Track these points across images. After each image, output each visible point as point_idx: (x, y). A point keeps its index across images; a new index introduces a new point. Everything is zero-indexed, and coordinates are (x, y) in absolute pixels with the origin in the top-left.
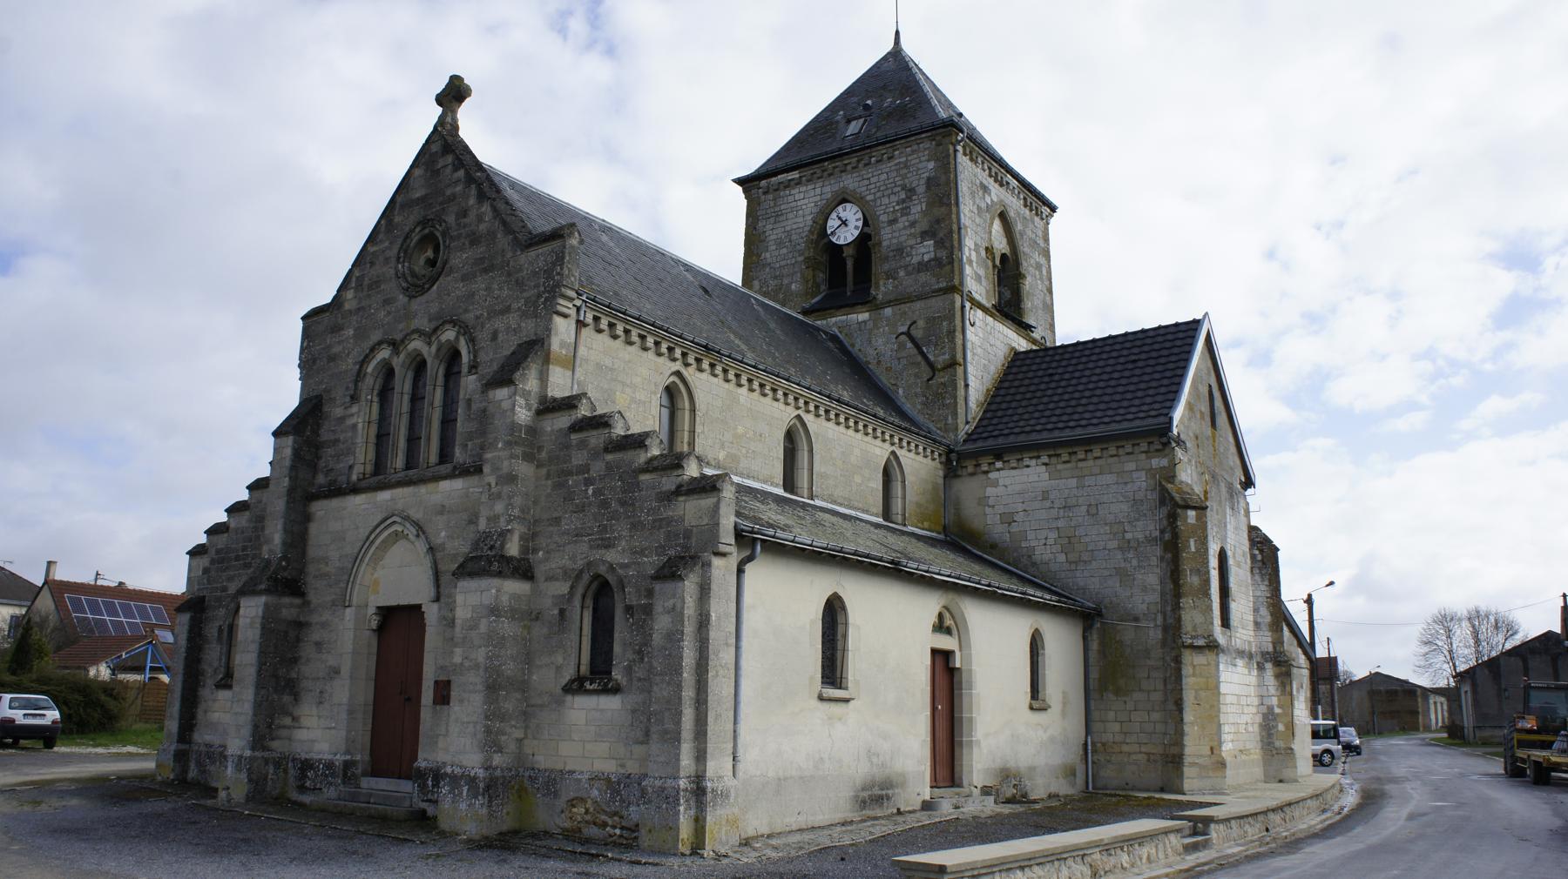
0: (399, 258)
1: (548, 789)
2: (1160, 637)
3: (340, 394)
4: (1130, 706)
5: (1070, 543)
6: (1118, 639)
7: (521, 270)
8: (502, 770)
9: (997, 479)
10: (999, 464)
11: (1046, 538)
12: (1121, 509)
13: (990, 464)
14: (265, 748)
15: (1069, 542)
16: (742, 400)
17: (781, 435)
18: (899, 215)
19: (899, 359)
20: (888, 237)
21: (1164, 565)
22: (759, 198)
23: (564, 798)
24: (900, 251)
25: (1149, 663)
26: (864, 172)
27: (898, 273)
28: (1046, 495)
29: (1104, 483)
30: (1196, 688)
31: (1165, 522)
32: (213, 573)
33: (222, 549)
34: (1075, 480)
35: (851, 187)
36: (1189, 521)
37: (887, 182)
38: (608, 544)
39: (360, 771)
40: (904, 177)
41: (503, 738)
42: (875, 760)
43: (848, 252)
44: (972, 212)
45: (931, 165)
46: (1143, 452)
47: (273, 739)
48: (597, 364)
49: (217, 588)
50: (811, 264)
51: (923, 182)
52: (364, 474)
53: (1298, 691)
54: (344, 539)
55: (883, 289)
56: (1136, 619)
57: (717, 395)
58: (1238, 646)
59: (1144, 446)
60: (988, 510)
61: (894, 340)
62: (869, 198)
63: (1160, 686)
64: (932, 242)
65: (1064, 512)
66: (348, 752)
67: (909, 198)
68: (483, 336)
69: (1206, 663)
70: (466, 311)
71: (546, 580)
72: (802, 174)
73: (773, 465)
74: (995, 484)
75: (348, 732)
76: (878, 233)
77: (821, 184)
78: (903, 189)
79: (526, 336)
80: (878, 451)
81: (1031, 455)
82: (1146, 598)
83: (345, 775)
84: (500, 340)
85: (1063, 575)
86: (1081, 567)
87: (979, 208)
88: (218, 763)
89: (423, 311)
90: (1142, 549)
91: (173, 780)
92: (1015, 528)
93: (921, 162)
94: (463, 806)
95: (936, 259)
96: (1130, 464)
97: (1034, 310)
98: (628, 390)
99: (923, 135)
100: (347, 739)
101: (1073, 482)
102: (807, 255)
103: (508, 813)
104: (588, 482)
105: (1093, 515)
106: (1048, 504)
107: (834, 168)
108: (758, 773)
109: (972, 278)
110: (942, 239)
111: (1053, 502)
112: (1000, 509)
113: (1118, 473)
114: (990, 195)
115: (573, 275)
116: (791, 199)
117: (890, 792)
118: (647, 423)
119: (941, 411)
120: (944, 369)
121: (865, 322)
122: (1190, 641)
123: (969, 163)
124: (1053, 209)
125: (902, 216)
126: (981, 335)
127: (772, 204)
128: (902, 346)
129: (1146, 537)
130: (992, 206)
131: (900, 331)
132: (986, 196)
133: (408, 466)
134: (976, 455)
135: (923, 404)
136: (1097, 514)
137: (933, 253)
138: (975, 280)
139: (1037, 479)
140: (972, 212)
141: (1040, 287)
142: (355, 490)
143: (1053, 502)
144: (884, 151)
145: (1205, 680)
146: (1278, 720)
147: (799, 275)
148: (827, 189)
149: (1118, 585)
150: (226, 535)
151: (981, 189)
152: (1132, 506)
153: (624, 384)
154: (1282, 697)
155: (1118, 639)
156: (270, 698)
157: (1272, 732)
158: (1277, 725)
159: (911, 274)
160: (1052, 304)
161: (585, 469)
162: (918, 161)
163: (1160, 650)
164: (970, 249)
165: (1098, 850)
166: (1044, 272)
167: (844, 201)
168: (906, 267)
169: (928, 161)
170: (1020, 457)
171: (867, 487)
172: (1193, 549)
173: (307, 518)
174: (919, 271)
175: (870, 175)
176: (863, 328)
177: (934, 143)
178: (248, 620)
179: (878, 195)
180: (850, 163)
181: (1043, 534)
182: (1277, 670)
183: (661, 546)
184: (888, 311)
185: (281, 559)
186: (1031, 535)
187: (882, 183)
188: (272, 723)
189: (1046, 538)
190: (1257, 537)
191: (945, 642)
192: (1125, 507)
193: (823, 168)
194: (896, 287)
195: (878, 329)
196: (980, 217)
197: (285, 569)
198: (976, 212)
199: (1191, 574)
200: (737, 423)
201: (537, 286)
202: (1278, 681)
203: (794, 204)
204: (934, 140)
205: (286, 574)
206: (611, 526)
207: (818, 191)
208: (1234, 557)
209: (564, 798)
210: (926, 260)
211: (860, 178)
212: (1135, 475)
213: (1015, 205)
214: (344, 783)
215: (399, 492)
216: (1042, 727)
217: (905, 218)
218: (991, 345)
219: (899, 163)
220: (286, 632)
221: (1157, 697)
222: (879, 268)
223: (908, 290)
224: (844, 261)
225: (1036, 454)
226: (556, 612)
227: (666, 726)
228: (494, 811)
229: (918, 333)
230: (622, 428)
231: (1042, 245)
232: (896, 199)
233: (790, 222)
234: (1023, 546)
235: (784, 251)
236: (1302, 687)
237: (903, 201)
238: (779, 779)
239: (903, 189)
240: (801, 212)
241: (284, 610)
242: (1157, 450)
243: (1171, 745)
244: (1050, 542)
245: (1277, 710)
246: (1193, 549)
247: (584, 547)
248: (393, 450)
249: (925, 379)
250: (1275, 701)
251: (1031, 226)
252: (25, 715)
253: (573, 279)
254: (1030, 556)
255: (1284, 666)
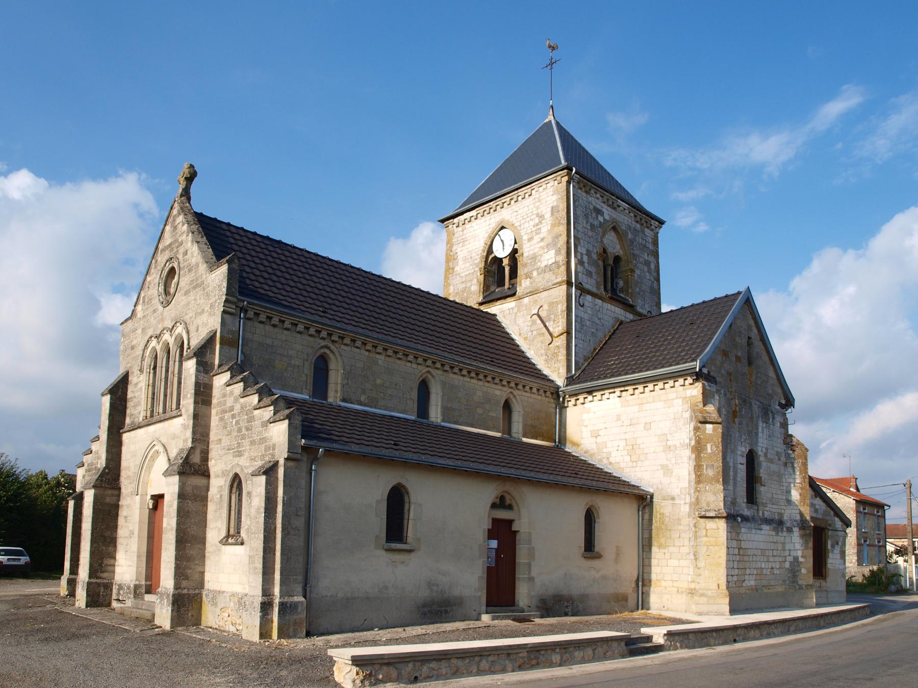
1: (213, 602)
2: (688, 510)
4: (668, 556)
6: (661, 511)
7: (208, 286)
14: (98, 578)
15: (633, 448)
16: (380, 362)
18: (534, 234)
19: (532, 331)
20: (527, 250)
22: (454, 230)
23: (219, 607)
24: (534, 258)
25: (680, 527)
30: (708, 544)
34: (637, 406)
35: (507, 218)
36: (707, 432)
37: (528, 212)
38: (239, 454)
42: (435, 588)
47: (103, 572)
53: (833, 546)
55: (523, 285)
56: (673, 499)
61: (529, 319)
62: (516, 225)
66: (137, 580)
70: (186, 314)
71: (215, 477)
78: (537, 216)
84: (199, 331)
85: (628, 470)
86: (639, 464)
87: (592, 226)
89: (170, 313)
95: (556, 262)
101: (636, 408)
103: (192, 616)
105: (648, 430)
106: (620, 423)
107: (497, 206)
108: (329, 595)
109: (583, 274)
110: (559, 248)
113: (664, 401)
114: (602, 215)
117: (449, 609)
118: (301, 379)
119: (556, 365)
123: (584, 194)
124: (662, 222)
128: (534, 323)
129: (681, 444)
130: (604, 223)
131: (533, 313)
132: (599, 216)
133: (164, 412)
136: (650, 429)
140: (585, 228)
144: (525, 192)
145: (715, 539)
146: (801, 566)
147: (476, 280)
152: (673, 423)
156: (100, 549)
157: (797, 574)
158: (801, 570)
159: (541, 274)
161: (232, 408)
165: (525, 650)
168: (538, 269)
172: (709, 451)
174: (545, 272)
175: (518, 209)
176: (511, 312)
177: (556, 182)
182: (802, 532)
183: (263, 455)
184: (526, 300)
186: (609, 444)
187: (525, 214)
188: (102, 563)
193: (490, 207)
194: (531, 283)
195: (520, 312)
196: (592, 231)
197: (108, 474)
198: (589, 228)
199: (706, 468)
201: (215, 296)
202: (803, 540)
204: (556, 180)
206: (242, 443)
207: (488, 223)
211: (512, 211)
213: (625, 219)
214: (135, 597)
218: (599, 319)
219: (535, 198)
221: (685, 550)
224: (504, 268)
226: (219, 496)
229: (543, 314)
231: (651, 247)
234: (604, 451)
235: (468, 264)
236: (837, 544)
237: (537, 225)
238: (348, 599)
239: (537, 216)
241: (107, 498)
243: (691, 582)
244: (621, 448)
245: (801, 559)
246: (709, 451)
247: (231, 457)
248: (157, 402)
250: (799, 553)
251: (641, 234)
252: (8, 559)
254: (608, 458)
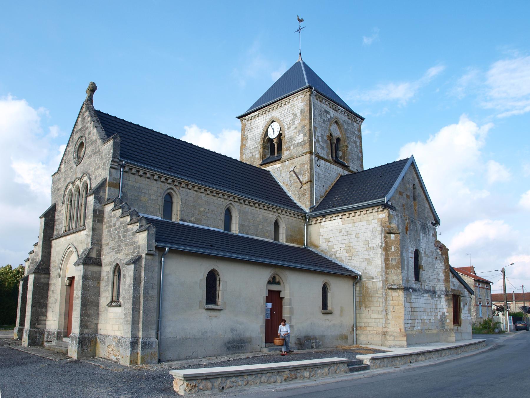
0: (74, 152)
1: (103, 342)
3: (60, 203)
5: (349, 249)
6: (366, 286)
8: (88, 335)
9: (324, 225)
10: (324, 219)
11: (341, 247)
12: (367, 235)
13: (321, 219)
14: (35, 328)
16: (203, 198)
17: (223, 211)
18: (291, 125)
19: (290, 181)
20: (287, 134)
21: (383, 257)
22: (245, 123)
24: (291, 138)
25: (377, 295)
26: (280, 109)
27: (290, 148)
28: (341, 231)
29: (362, 225)
31: (383, 239)
35: (275, 116)
36: (392, 239)
37: (287, 113)
38: (119, 252)
39: (63, 335)
40: (293, 110)
41: (89, 323)
42: (235, 332)
43: (275, 141)
44: (320, 122)
45: (302, 104)
46: (376, 212)
47: (39, 324)
48: (132, 186)
50: (264, 147)
51: (299, 111)
52: (66, 230)
53: (464, 306)
55: (285, 154)
56: (373, 278)
57: (190, 196)
58: (426, 289)
59: (376, 209)
60: (321, 237)
61: (289, 174)
63: (381, 305)
64: (302, 134)
65: (347, 237)
66: (59, 329)
67: (295, 118)
68: (93, 178)
69: (398, 295)
72: (259, 113)
73: (218, 222)
74: (323, 227)
75: (59, 321)
76: (284, 133)
77: (265, 116)
78: (292, 115)
79: (103, 177)
80: (271, 216)
81: (336, 215)
82: (376, 270)
83: (58, 336)
84: (97, 179)
85: (347, 261)
87: (324, 120)
89: (80, 169)
90: (375, 250)
91: (18, 339)
92: (330, 244)
93: (299, 103)
95: (303, 141)
96: (371, 217)
97: (352, 159)
98: (147, 196)
99: (299, 93)
100: (59, 324)
101: (350, 225)
102: (261, 143)
104: (116, 229)
106: (341, 234)
107: (270, 109)
109: (319, 148)
111: (343, 233)
112: (325, 237)
114: (330, 114)
115: (117, 153)
116: (256, 122)
119: (304, 200)
120: (305, 183)
121: (279, 168)
122: (391, 287)
123: (319, 102)
124: (363, 119)
125: (292, 125)
126: (323, 170)
127: (250, 125)
128: (291, 176)
129: (377, 246)
130: (331, 119)
131: (291, 170)
134: (316, 217)
135: (298, 198)
137: (302, 139)
138: (321, 148)
139: (338, 225)
141: (356, 150)
142: (62, 237)
143: (343, 233)
145: (397, 302)
146: (447, 318)
147: (258, 151)
148: (267, 117)
149: (366, 265)
150: (33, 254)
151: (325, 112)
153: (145, 193)
154: (448, 309)
155: (366, 286)
158: (446, 320)
160: (362, 157)
162: (297, 103)
163: (381, 290)
164: (318, 136)
165: (288, 370)
166: (358, 144)
167: (273, 121)
168: (293, 145)
169: (301, 103)
170: (331, 216)
171: (266, 230)
172: (393, 250)
173: (50, 247)
177: (303, 95)
179: (284, 118)
180: (275, 107)
181: (339, 246)
182: (447, 298)
184: (287, 163)
185: (41, 262)
187: (286, 113)
188: (38, 319)
189: (341, 247)
190: (439, 245)
191: (274, 288)
192: (369, 234)
197: (42, 265)
200: (200, 207)
201: (106, 158)
202: (447, 302)
203: (257, 124)
205: (43, 267)
207: (265, 118)
208: (425, 253)
209: (107, 345)
210: (300, 142)
211: (278, 112)
212: (373, 221)
216: (329, 320)
217: (293, 126)
220: (43, 287)
222: (284, 146)
223: (294, 154)
224: (274, 144)
225: (337, 215)
227: (128, 319)
228: (84, 349)
229: (297, 171)
230: (127, 209)
232: (290, 119)
233: (255, 131)
235: (253, 142)
237: (293, 120)
238: (183, 339)
239: (292, 115)
240: (259, 127)
242: (381, 211)
243: (384, 328)
244: (342, 249)
245: (446, 314)
246: (393, 250)
249: (299, 188)
250: (445, 310)
251: (351, 126)
253: (117, 155)
254: (335, 255)
255: (450, 296)
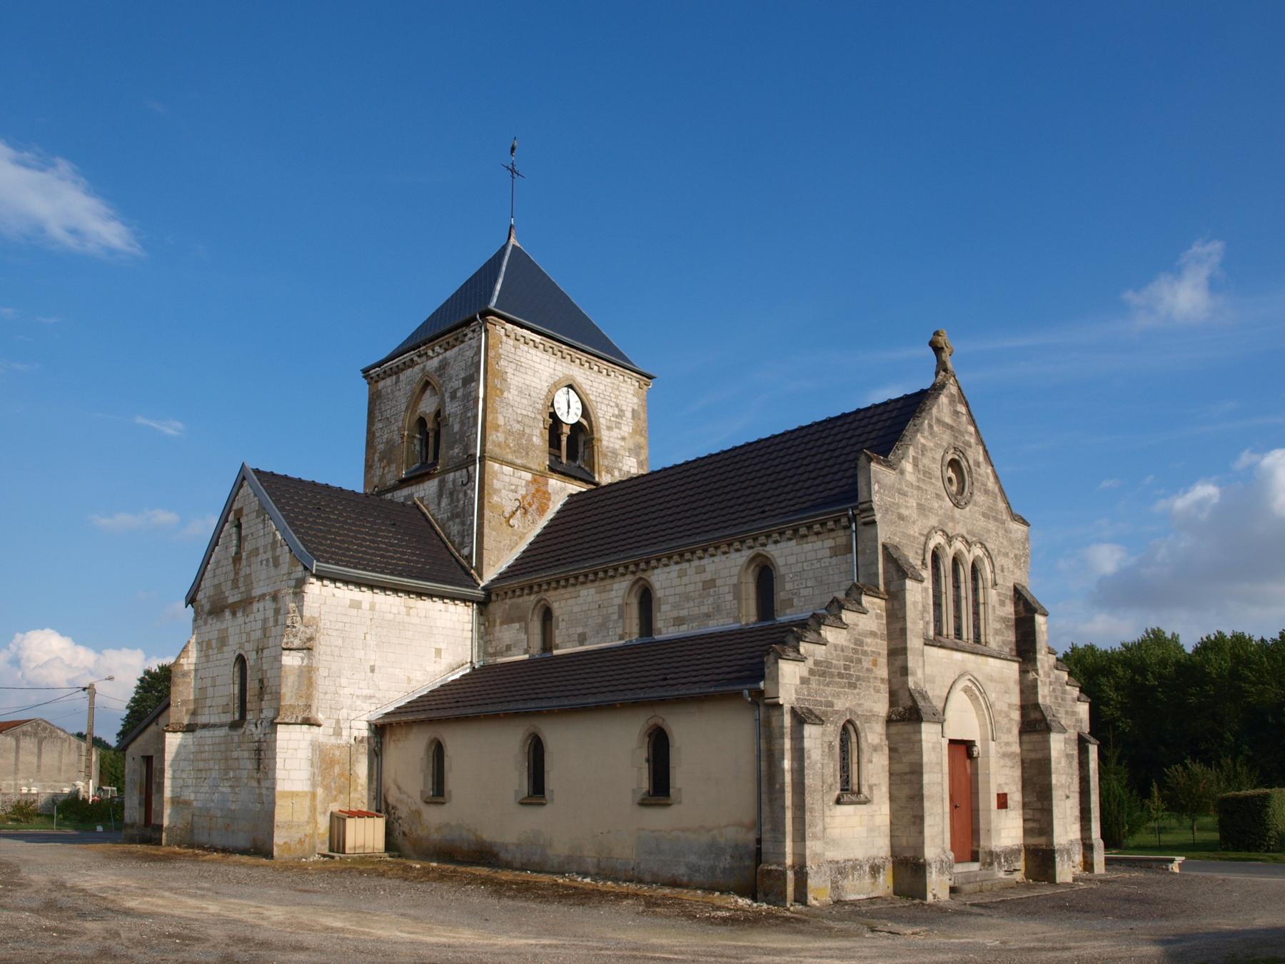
32: (814, 685)
33: (821, 662)
49: (821, 701)
54: (934, 682)
88: (850, 877)
94: (1066, 866)
178: (931, 745)
215: (966, 655)
